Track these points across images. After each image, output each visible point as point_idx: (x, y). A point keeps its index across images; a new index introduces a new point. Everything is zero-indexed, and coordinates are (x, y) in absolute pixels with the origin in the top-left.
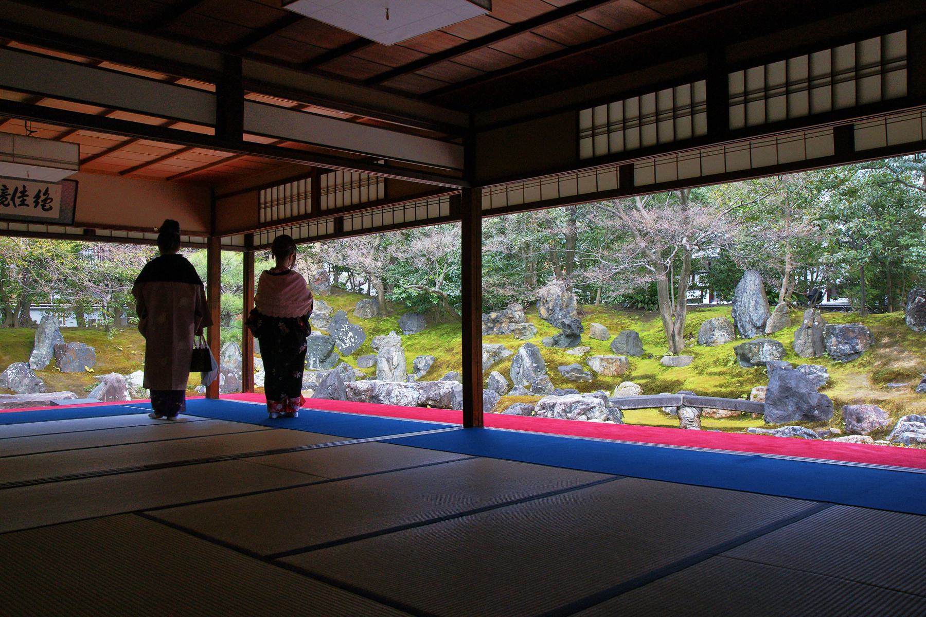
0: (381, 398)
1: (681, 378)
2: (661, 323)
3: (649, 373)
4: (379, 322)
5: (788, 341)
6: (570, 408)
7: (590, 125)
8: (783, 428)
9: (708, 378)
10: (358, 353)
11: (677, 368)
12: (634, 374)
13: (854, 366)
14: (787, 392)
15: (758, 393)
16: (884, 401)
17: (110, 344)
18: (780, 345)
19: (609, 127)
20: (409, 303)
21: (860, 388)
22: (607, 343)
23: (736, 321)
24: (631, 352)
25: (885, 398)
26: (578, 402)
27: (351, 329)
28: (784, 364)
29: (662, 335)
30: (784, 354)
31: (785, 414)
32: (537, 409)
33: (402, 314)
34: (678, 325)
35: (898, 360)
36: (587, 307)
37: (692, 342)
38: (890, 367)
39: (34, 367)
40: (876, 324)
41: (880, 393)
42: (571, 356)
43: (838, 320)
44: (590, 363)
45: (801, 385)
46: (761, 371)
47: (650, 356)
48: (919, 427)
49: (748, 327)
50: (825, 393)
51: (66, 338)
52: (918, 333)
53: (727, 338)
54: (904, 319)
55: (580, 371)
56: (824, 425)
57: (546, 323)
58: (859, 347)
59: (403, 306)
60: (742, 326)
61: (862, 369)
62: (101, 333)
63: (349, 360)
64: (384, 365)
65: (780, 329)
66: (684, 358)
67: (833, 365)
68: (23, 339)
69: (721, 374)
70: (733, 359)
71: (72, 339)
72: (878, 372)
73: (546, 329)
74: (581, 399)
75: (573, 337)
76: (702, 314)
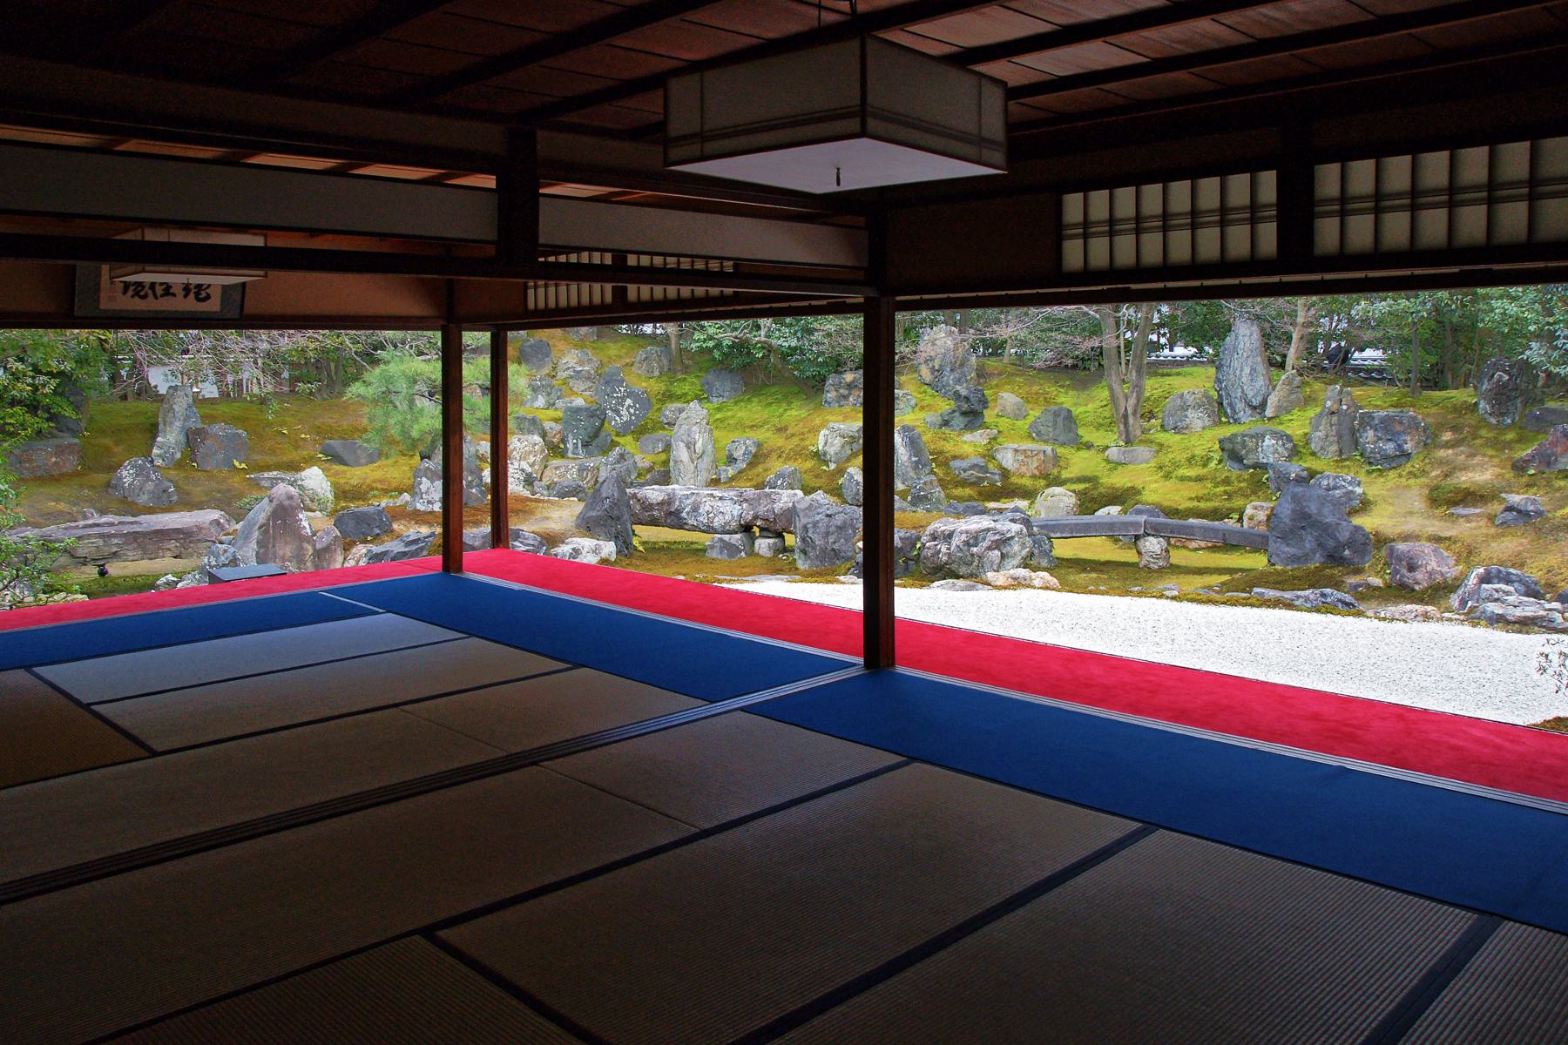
0: (684, 515)
1: (1138, 484)
2: (1106, 393)
3: (1088, 473)
4: (672, 383)
5: (1300, 432)
6: (976, 538)
7: (1079, 218)
8: (1307, 592)
9: (1179, 485)
10: (640, 430)
11: (1131, 467)
12: (1065, 475)
13: (1400, 476)
14: (1304, 520)
15: (1256, 511)
16: (1449, 539)
17: (269, 425)
18: (1289, 438)
19: (1112, 226)
20: (717, 354)
21: (1411, 513)
22: (1024, 424)
23: (1220, 396)
24: (1061, 439)
25: (1448, 534)
26: (988, 530)
27: (630, 395)
28: (1294, 469)
29: (1107, 414)
30: (1294, 453)
31: (1299, 553)
32: (924, 539)
33: (707, 370)
34: (1132, 401)
35: (1465, 468)
36: (992, 363)
37: (1154, 426)
38: (1455, 481)
39: (159, 462)
40: (1434, 410)
41: (1442, 524)
42: (970, 444)
43: (1374, 399)
44: (999, 457)
45: (1326, 511)
46: (1260, 479)
47: (1089, 446)
48: (1507, 593)
49: (1240, 406)
50: (1357, 521)
51: (204, 418)
52: (1496, 427)
53: (1207, 422)
54: (1476, 404)
55: (984, 469)
56: (1358, 571)
57: (929, 390)
58: (1408, 447)
59: (707, 357)
60: (1230, 404)
61: (1412, 481)
62: (255, 407)
63: (627, 442)
64: (681, 453)
65: (1288, 412)
66: (1142, 451)
67: (1369, 473)
68: (141, 419)
69: (1199, 479)
70: (1217, 456)
71: (210, 419)
72: (1436, 488)
73: (928, 400)
74: (993, 525)
75: (972, 415)
76: (1167, 380)
